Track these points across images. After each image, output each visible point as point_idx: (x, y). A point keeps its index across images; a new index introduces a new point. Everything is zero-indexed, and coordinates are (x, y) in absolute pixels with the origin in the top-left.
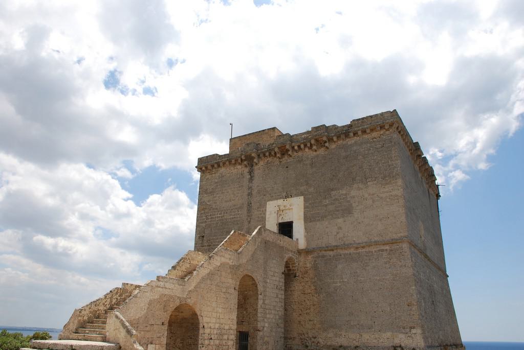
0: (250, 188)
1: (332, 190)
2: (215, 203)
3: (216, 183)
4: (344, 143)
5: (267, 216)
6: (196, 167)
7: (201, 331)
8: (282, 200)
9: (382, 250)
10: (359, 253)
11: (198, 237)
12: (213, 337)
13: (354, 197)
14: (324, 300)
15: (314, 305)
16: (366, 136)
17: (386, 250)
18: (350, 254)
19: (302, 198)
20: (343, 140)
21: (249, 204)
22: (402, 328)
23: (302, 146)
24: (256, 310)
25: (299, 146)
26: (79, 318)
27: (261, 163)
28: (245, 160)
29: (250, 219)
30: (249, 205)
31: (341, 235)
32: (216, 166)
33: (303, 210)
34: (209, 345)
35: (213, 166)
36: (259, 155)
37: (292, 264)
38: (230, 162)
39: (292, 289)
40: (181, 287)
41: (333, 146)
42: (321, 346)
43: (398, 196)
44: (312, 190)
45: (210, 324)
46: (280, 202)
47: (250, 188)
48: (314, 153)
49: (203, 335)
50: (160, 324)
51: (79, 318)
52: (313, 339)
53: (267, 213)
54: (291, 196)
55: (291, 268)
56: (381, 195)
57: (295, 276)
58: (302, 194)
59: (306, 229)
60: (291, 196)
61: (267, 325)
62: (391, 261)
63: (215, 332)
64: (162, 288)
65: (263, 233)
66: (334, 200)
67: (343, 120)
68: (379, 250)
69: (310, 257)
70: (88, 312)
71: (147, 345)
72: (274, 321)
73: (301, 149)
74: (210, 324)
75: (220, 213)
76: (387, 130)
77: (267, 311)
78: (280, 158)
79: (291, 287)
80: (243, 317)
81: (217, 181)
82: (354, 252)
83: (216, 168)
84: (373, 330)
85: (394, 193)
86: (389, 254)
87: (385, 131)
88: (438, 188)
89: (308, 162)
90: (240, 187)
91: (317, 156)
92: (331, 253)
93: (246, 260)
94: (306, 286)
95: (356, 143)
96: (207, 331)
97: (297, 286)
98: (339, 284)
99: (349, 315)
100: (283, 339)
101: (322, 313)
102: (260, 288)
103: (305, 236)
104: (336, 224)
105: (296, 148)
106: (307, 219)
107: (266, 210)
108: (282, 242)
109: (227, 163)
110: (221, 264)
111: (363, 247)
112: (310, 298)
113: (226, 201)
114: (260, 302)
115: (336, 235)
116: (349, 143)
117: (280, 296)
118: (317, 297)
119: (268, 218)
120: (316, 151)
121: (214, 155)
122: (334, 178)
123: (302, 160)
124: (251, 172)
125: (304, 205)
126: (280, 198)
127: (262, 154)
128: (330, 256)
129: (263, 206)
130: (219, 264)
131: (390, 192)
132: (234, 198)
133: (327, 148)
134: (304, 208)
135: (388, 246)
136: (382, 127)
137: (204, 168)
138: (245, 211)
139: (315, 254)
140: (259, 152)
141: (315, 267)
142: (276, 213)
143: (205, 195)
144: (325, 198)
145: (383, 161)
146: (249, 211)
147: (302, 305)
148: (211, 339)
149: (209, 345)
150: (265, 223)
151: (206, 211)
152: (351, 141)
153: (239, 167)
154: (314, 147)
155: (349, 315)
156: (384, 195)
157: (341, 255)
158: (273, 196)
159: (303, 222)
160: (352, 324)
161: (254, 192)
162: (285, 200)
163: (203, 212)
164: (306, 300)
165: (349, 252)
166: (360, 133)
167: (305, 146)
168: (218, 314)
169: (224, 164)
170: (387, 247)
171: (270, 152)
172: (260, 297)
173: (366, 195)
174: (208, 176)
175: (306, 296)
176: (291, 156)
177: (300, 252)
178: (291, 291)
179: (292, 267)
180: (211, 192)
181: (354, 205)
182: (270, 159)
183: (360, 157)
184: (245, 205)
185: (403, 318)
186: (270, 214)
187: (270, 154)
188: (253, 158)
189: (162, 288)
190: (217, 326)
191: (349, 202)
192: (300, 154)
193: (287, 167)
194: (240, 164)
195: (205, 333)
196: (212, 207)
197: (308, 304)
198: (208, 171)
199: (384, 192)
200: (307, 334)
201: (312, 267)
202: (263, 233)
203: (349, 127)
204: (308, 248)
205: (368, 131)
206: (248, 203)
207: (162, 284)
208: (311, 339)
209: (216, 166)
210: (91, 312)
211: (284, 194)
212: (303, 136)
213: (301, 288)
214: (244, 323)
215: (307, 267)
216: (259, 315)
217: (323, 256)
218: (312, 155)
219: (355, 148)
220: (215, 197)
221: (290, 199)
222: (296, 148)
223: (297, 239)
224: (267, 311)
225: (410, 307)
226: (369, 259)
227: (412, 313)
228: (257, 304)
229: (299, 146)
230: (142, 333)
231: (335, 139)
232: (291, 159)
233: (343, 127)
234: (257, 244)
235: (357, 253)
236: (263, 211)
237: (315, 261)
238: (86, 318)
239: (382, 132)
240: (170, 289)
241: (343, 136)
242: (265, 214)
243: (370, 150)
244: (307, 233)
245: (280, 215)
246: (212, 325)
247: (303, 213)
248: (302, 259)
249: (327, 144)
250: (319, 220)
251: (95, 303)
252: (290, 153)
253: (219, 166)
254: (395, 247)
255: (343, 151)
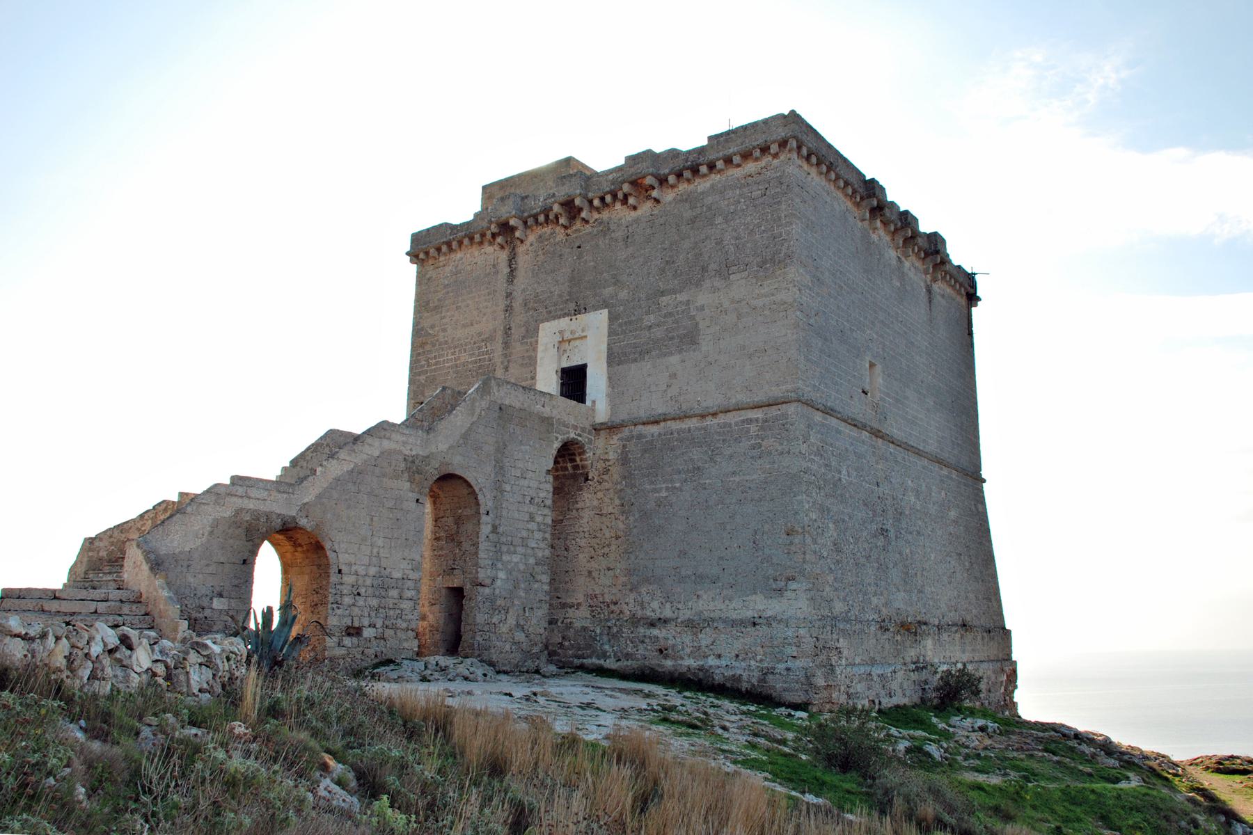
0: (509, 295)
1: (663, 293)
2: (444, 330)
3: (446, 286)
4: (691, 187)
5: (539, 355)
6: (408, 254)
7: (334, 578)
8: (567, 319)
9: (750, 421)
10: (705, 429)
11: (412, 405)
12: (362, 591)
13: (702, 308)
14: (635, 527)
15: (617, 538)
16: (715, 178)
17: (757, 420)
18: (689, 429)
19: (605, 312)
20: (688, 181)
21: (507, 330)
22: (772, 580)
23: (608, 198)
24: (476, 545)
25: (602, 199)
26: (91, 554)
27: (532, 238)
28: (499, 234)
29: (508, 361)
30: (506, 333)
31: (673, 391)
32: (444, 248)
33: (605, 339)
34: (354, 605)
35: (439, 250)
36: (525, 223)
37: (580, 454)
38: (471, 239)
39: (579, 505)
40: (285, 496)
41: (668, 196)
42: (625, 619)
43: (785, 303)
44: (623, 294)
45: (354, 568)
46: (564, 323)
47: (509, 295)
48: (633, 214)
49: (338, 586)
50: (237, 562)
51: (91, 554)
52: (612, 607)
53: (540, 348)
54: (585, 309)
55: (579, 462)
56: (754, 303)
57: (587, 479)
58: (605, 305)
59: (609, 378)
60: (585, 309)
61: (502, 575)
62: (764, 443)
63: (369, 582)
64: (242, 497)
65: (495, 389)
66: (665, 316)
67: (691, 138)
68: (743, 421)
69: (615, 440)
70: (107, 544)
71: (211, 599)
72: (522, 567)
73: (607, 205)
74: (354, 568)
75: (452, 351)
76: (776, 156)
77: (504, 548)
78: (566, 227)
79: (577, 502)
80: (454, 560)
81: (446, 282)
82: (697, 425)
83: (445, 254)
84: (720, 584)
85: (778, 298)
86: (762, 428)
87: (770, 158)
88: (973, 278)
89: (619, 234)
90: (489, 294)
91: (637, 221)
92: (654, 429)
93: (446, 446)
94: (606, 500)
95: (712, 186)
96: (349, 579)
97: (588, 499)
98: (664, 494)
99: (679, 556)
100: (545, 606)
101: (631, 553)
102: (486, 501)
103: (608, 395)
104: (667, 367)
105: (596, 202)
106: (614, 358)
107: (537, 342)
108: (547, 409)
109: (466, 241)
110: (382, 453)
111: (714, 415)
112: (611, 522)
113: (464, 326)
114: (485, 530)
115: (666, 391)
116: (700, 188)
117: (539, 519)
118: (623, 521)
119: (542, 358)
120: (635, 208)
121: (441, 225)
122: (668, 267)
123: (609, 229)
124: (512, 260)
125: (609, 328)
126: (565, 315)
127: (531, 220)
128: (653, 436)
129: (531, 333)
130: (377, 453)
131: (773, 295)
132: (478, 319)
133: (657, 201)
134: (609, 336)
135: (761, 410)
136: (765, 150)
137: (422, 256)
138: (498, 346)
139: (626, 432)
140: (526, 214)
141: (624, 460)
142: (556, 347)
143: (426, 314)
144: (648, 313)
145: (763, 228)
146: (506, 345)
147: (595, 537)
148: (359, 594)
149: (354, 605)
150: (535, 369)
151: (428, 347)
152: (702, 185)
153: (489, 249)
154: (631, 201)
155: (679, 556)
156: (758, 303)
157: (672, 434)
158: (550, 312)
159: (606, 364)
160: (683, 573)
161: (517, 305)
162: (574, 318)
163: (421, 351)
164: (604, 527)
165: (687, 426)
166: (720, 164)
167: (615, 196)
168: (375, 551)
169: (460, 243)
170: (759, 414)
171: (546, 217)
172: (484, 518)
173: (726, 304)
174: (431, 273)
175: (604, 519)
176: (587, 222)
177: (597, 429)
178: (577, 510)
179: (581, 461)
180: (436, 308)
181: (702, 325)
182: (547, 230)
183: (719, 220)
184: (500, 333)
185: (775, 561)
186: (546, 349)
187: (547, 217)
188: (513, 229)
189: (242, 497)
190: (372, 571)
191: (693, 318)
192: (605, 215)
193: (579, 247)
194: (491, 244)
195: (342, 584)
196: (437, 340)
197: (608, 535)
198: (431, 262)
199: (759, 296)
200: (603, 595)
201: (618, 459)
202: (495, 389)
203: (700, 153)
204: (613, 419)
205: (737, 159)
206: (505, 327)
207: (240, 491)
208: (608, 606)
209: (444, 248)
210: (112, 544)
211: (572, 306)
212: (610, 177)
213: (595, 503)
214: (455, 572)
215: (608, 460)
216: (482, 555)
217: (640, 437)
218: (629, 219)
219: (709, 200)
220: (444, 317)
221: (582, 316)
222: (596, 202)
223: (594, 402)
224: (504, 548)
225: (790, 538)
226: (723, 440)
227: (793, 548)
228: (478, 533)
229: (602, 199)
230: (200, 576)
231: (672, 179)
232: (588, 228)
233: (690, 152)
234: (478, 411)
235: (702, 428)
236: (531, 343)
237: (624, 446)
238: (103, 554)
239: (763, 163)
240: (258, 499)
241: (687, 174)
242: (535, 350)
243: (740, 203)
244: (613, 388)
245: (565, 351)
246: (361, 571)
247: (606, 346)
248: (600, 442)
249: (655, 194)
250: (635, 360)
251: (120, 528)
252: (583, 215)
253: (451, 249)
254: (774, 412)
255: (687, 205)
